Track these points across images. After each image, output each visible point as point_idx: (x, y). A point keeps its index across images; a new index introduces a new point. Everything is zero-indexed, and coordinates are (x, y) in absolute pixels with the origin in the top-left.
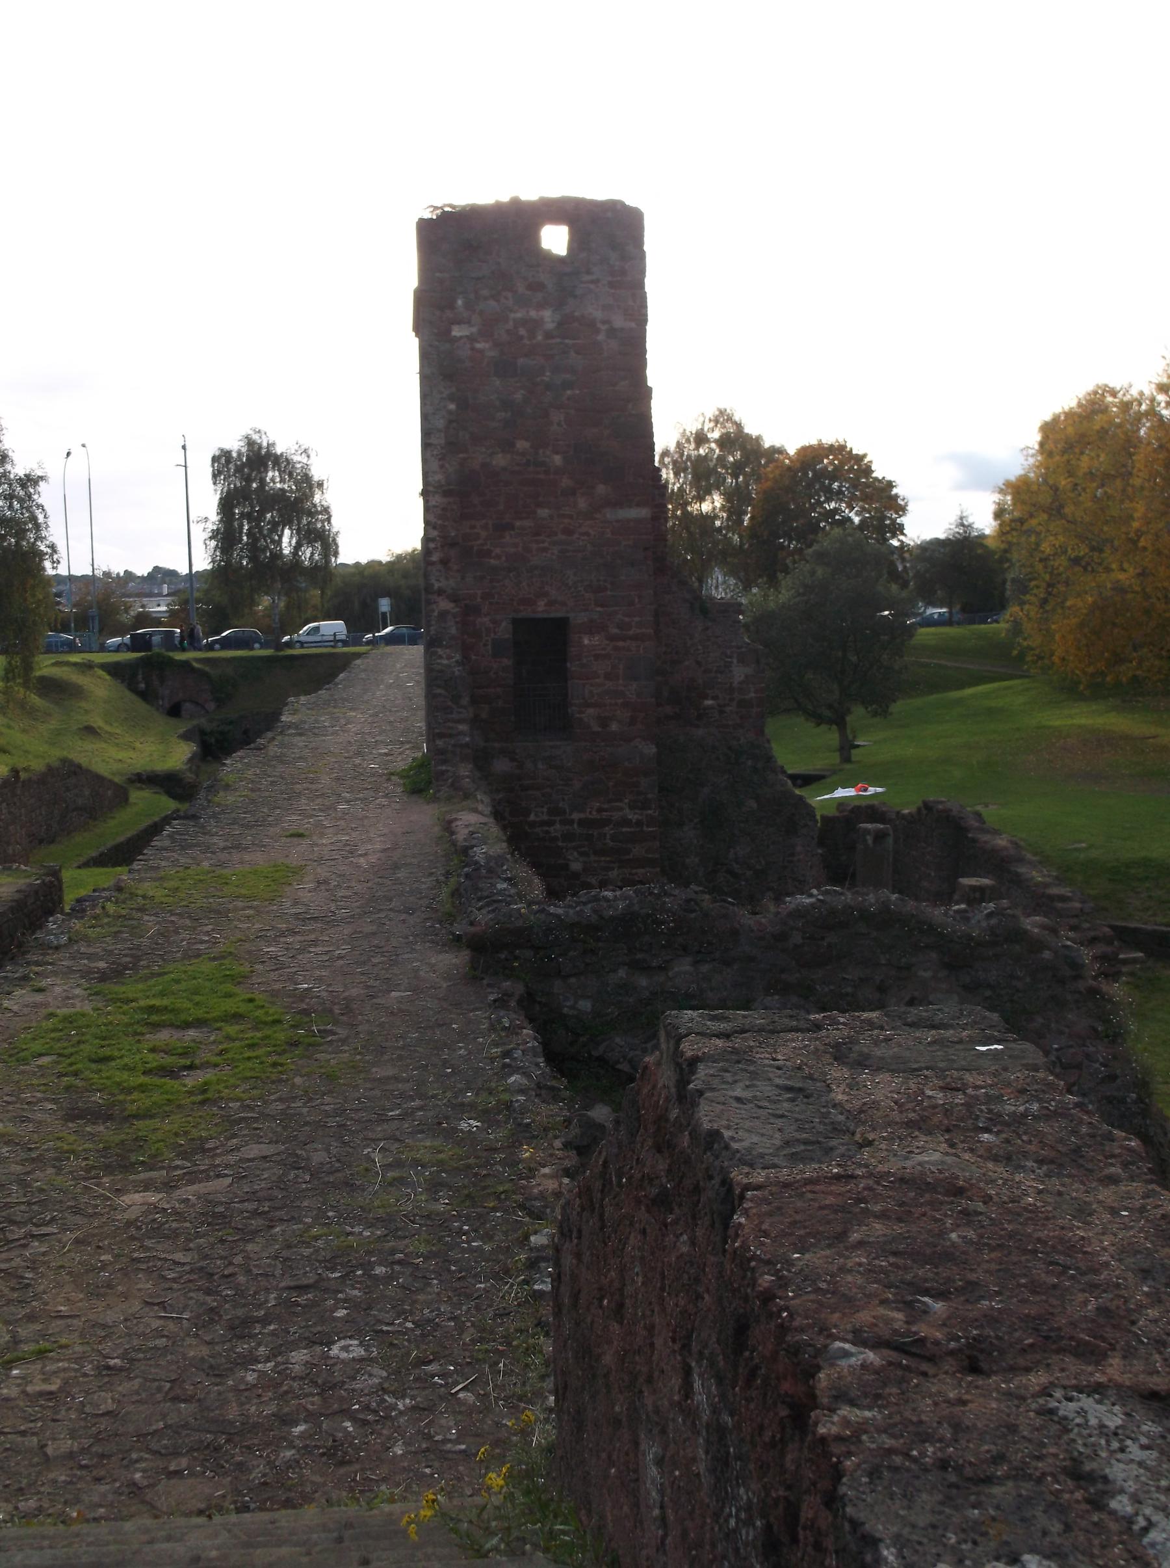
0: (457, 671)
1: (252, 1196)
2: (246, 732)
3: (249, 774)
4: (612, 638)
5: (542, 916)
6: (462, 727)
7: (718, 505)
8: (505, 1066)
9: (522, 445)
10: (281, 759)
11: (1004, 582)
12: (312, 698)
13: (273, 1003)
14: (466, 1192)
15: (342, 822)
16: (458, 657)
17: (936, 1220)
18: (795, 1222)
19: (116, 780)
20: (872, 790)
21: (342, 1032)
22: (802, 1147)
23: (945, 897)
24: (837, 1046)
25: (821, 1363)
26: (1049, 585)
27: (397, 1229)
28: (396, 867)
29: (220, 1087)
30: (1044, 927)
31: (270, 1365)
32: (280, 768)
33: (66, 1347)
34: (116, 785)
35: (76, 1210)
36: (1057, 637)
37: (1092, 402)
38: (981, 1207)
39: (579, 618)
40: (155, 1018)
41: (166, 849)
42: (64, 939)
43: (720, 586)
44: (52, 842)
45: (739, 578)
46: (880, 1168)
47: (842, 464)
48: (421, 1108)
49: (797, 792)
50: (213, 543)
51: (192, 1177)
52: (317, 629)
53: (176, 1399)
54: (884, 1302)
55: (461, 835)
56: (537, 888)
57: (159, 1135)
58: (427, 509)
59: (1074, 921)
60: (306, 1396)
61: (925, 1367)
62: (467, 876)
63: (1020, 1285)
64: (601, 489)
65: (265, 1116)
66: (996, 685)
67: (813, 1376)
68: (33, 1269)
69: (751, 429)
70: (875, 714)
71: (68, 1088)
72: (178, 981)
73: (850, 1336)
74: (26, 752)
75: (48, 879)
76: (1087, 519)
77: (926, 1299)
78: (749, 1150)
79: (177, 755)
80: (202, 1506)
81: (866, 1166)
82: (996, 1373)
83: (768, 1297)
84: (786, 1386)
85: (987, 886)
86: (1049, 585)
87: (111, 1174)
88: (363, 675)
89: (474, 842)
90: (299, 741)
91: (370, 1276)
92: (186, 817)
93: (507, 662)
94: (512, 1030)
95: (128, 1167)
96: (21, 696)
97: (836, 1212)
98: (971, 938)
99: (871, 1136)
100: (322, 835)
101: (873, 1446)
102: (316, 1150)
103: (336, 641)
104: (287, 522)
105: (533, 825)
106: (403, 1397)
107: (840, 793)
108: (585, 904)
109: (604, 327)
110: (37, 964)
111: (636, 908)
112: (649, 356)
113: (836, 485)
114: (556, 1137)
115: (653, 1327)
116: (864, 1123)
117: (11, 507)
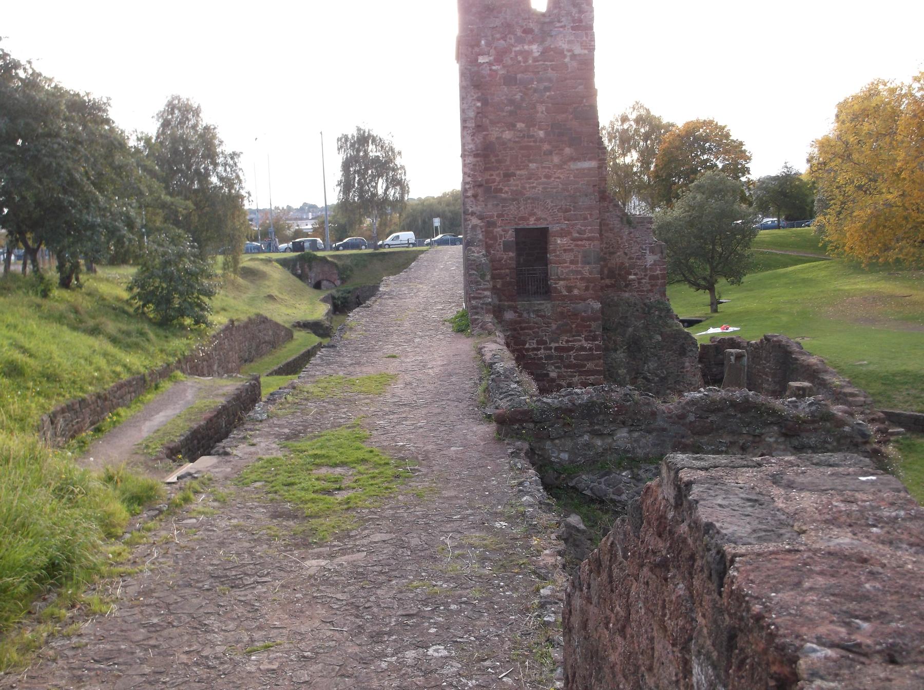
0: (483, 260)
1: (378, 563)
2: (358, 297)
3: (363, 321)
5: (539, 404)
6: (487, 293)
8: (520, 491)
9: (520, 125)
10: (380, 312)
11: (813, 202)
12: (397, 277)
13: (384, 453)
14: (501, 563)
15: (417, 349)
16: (484, 252)
17: (855, 577)
18: (769, 576)
19: (287, 325)
20: (731, 329)
21: (424, 470)
23: (779, 393)
24: (773, 476)
25: (800, 655)
27: (462, 584)
28: (450, 375)
29: (357, 501)
30: (845, 412)
32: (381, 318)
33: (280, 644)
34: (286, 329)
35: (281, 569)
37: (870, 90)
38: (881, 570)
40: (318, 461)
41: (318, 365)
42: (265, 416)
43: (636, 207)
44: (252, 361)
45: (647, 202)
46: (814, 546)
47: (711, 132)
49: (686, 330)
50: (339, 188)
51: (344, 552)
52: (398, 237)
53: (343, 676)
54: (832, 622)
55: (488, 357)
56: (534, 388)
57: (324, 527)
58: (464, 165)
59: (861, 409)
60: (416, 676)
61: (862, 659)
62: (493, 380)
63: (913, 615)
64: (568, 151)
65: (383, 518)
66: (807, 265)
67: (795, 662)
68: (259, 601)
69: (655, 112)
70: (733, 283)
71: (271, 500)
72: (329, 440)
73: (815, 641)
77: (857, 621)
78: (733, 534)
79: (320, 311)
81: (806, 545)
82: (906, 664)
83: (759, 618)
84: (774, 669)
85: (807, 387)
87: (299, 549)
89: (496, 360)
90: (390, 302)
91: (448, 610)
92: (329, 347)
94: (523, 470)
95: (307, 545)
97: (793, 570)
98: (798, 418)
99: (804, 528)
100: (406, 357)
102: (413, 537)
103: (409, 244)
104: (380, 175)
105: (527, 350)
106: (471, 679)
107: (712, 331)
108: (564, 396)
109: (569, 54)
110: (251, 430)
111: (595, 399)
112: (596, 70)
113: (707, 145)
114: (552, 533)
116: (798, 520)
117: (225, 170)
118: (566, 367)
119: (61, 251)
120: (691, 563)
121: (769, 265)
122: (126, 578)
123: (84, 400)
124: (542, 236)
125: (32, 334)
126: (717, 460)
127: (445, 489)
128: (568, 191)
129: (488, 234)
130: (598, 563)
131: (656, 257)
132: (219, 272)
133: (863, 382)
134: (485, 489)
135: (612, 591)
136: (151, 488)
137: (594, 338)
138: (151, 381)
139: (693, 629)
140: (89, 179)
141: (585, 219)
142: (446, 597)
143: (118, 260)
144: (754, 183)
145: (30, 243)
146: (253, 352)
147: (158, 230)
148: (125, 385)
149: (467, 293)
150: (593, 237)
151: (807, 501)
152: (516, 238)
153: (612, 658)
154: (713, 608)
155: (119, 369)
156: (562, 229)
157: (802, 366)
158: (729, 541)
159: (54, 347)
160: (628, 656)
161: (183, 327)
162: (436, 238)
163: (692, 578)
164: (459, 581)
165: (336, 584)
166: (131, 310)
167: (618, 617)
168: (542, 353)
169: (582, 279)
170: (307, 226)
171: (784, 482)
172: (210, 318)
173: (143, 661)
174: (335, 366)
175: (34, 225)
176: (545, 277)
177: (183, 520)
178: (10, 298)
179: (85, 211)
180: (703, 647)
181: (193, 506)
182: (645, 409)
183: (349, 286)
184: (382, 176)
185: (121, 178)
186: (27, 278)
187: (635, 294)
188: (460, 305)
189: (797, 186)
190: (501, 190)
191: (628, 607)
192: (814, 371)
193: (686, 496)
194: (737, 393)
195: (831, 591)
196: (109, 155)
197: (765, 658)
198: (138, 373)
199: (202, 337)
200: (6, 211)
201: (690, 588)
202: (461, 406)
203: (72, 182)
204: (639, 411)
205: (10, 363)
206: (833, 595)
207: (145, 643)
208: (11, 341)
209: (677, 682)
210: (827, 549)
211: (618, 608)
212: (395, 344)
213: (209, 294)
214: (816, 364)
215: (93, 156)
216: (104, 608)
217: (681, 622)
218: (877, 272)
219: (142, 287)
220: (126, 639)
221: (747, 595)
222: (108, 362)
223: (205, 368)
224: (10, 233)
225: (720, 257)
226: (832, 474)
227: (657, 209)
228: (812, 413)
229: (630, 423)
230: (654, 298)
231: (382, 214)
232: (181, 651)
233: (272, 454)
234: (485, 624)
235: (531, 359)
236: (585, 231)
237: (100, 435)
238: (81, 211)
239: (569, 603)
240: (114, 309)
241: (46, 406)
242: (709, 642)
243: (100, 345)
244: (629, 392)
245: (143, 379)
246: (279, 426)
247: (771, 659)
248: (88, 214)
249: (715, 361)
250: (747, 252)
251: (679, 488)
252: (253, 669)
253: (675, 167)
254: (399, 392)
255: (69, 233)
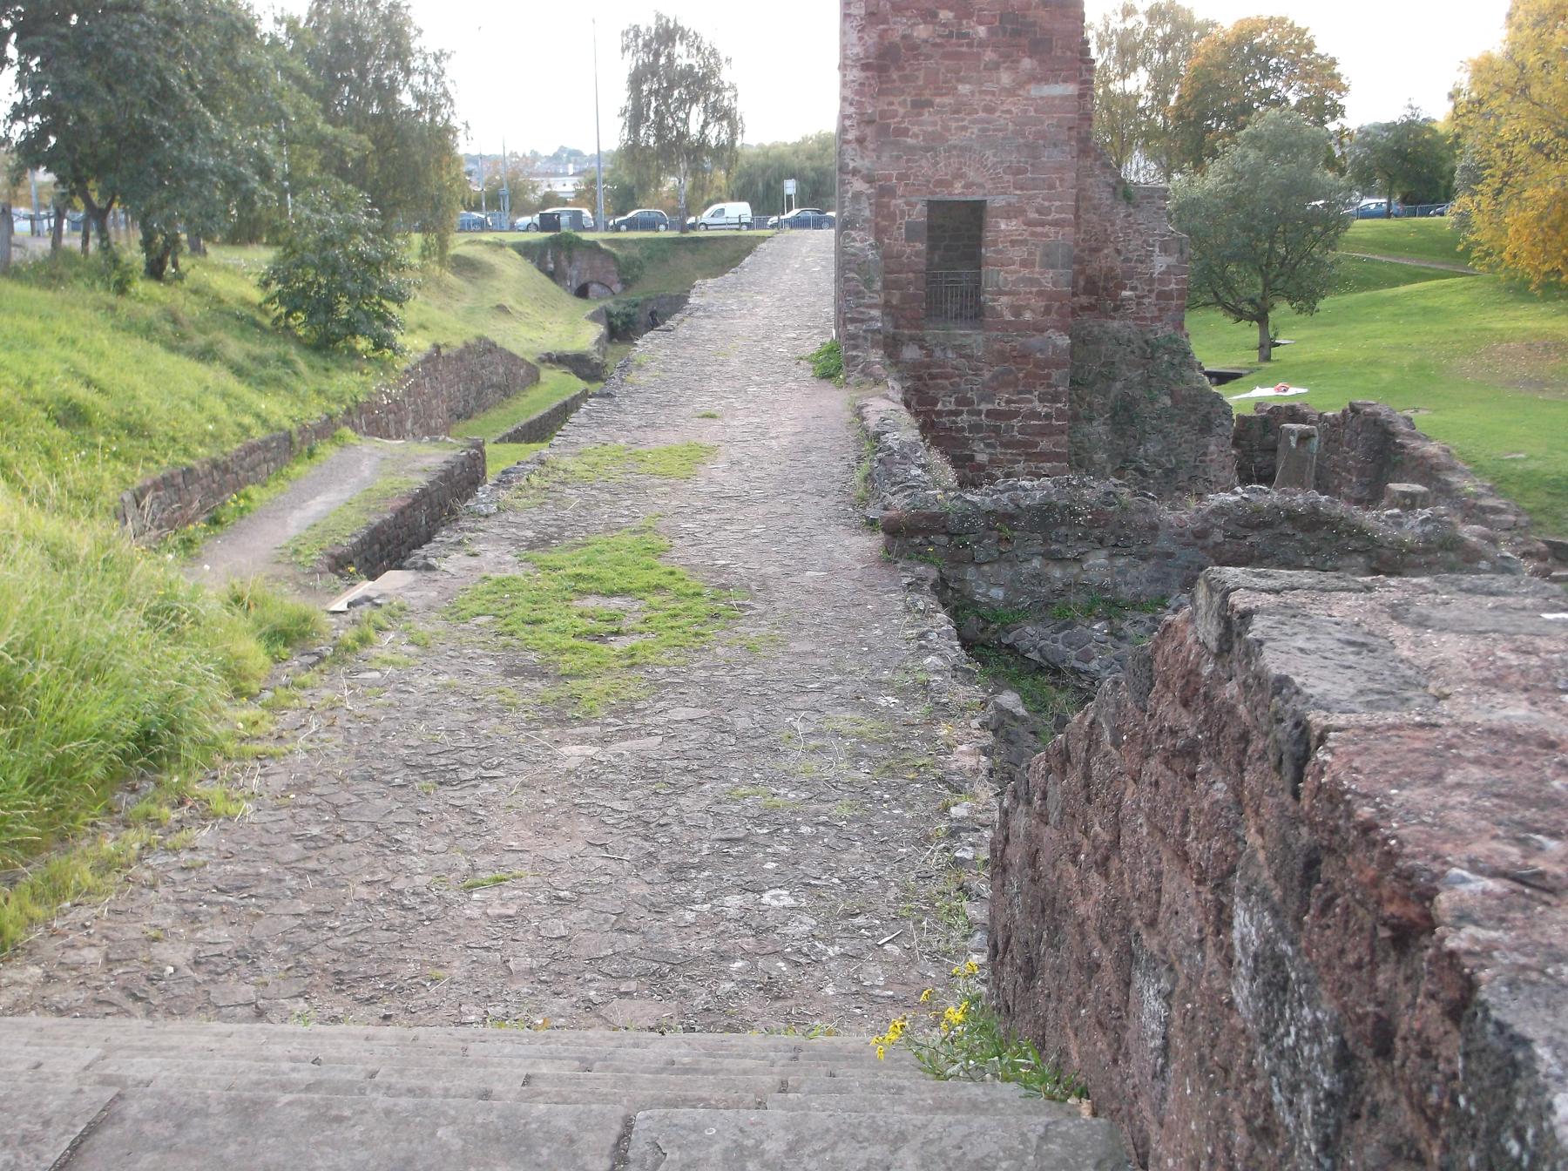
0: (871, 255)
3: (660, 355)
4: (1029, 224)
5: (958, 503)
6: (875, 313)
7: (1143, 83)
8: (921, 647)
9: (945, 15)
10: (689, 340)
11: (1453, 171)
14: (886, 763)
15: (752, 405)
16: (872, 240)
17: (1535, 769)
19: (529, 359)
20: (1292, 391)
21: (761, 607)
22: (1377, 697)
24: (1392, 606)
26: (1506, 174)
27: (821, 793)
28: (807, 451)
30: (1483, 537)
31: (707, 906)
32: (691, 350)
36: (1510, 232)
39: (997, 202)
40: (582, 585)
42: (493, 508)
43: (1139, 169)
44: (470, 417)
46: (1464, 719)
47: (1282, 38)
48: (839, 683)
49: (1214, 389)
51: (625, 734)
54: (1495, 837)
55: (872, 422)
56: (950, 476)
57: (592, 694)
58: (844, 85)
60: (741, 936)
61: (1546, 897)
64: (1027, 63)
66: (1434, 283)
67: (1431, 899)
70: (1300, 311)
71: (505, 647)
72: (601, 552)
73: (1466, 865)
74: (445, 329)
75: (473, 451)
76: (1555, 101)
77: (1539, 837)
78: (1324, 695)
79: (586, 336)
80: (652, 1025)
83: (1368, 828)
84: (1391, 909)
86: (1506, 174)
88: (769, 259)
92: (601, 396)
93: (920, 246)
95: (564, 722)
96: (437, 273)
97: (1427, 755)
98: (1402, 543)
99: (1447, 690)
100: (733, 417)
101: (1506, 962)
104: (694, 100)
105: (939, 414)
106: (833, 944)
107: (1259, 393)
108: (1002, 492)
110: (471, 530)
113: (1273, 62)
114: (973, 717)
115: (1160, 873)
116: (1437, 678)
117: (425, 82)
118: (1003, 445)
119: (147, 215)
120: (1242, 746)
121: (1370, 279)
122: (266, 762)
123: (190, 470)
124: (975, 213)
125: (102, 354)
126: (1295, 579)
127: (792, 639)
128: (1024, 136)
129: (880, 208)
130: (1065, 756)
131: (1172, 260)
132: (416, 261)
133: (1515, 490)
134: (861, 641)
135: (1089, 800)
136: (306, 620)
137: (1055, 399)
138: (302, 442)
139: (1238, 855)
140: (193, 88)
141: (1052, 187)
142: (794, 813)
143: (241, 236)
144: (1350, 135)
145: (95, 197)
146: (472, 402)
147: (313, 184)
148: (259, 448)
149: (839, 311)
150: (1064, 220)
151: (1451, 648)
152: (929, 216)
153: (1081, 910)
154: (1279, 818)
155: (247, 420)
156: (1009, 204)
157: (1413, 458)
158: (1317, 706)
159: (138, 380)
160: (1112, 905)
161: (354, 354)
162: (788, 216)
163: (1243, 771)
164: (817, 790)
165: (611, 785)
166: (267, 322)
167: (1098, 843)
168: (964, 420)
169: (1040, 294)
170: (565, 186)
171: (1412, 617)
172: (400, 340)
173: (297, 894)
174: (611, 429)
175: (102, 168)
176: (977, 288)
177: (359, 672)
178: (64, 293)
179: (187, 146)
180: (1256, 882)
181: (374, 652)
182: (1140, 519)
183: (637, 295)
184: (697, 101)
185: (248, 88)
186: (90, 260)
187: (1130, 323)
188: (824, 333)
189: (1427, 141)
190: (905, 132)
191: (1117, 826)
192: (1432, 467)
193: (1239, 635)
194: (1300, 498)
195: (1495, 790)
196: (227, 48)
197: (1375, 892)
198: (281, 429)
199: (386, 372)
200: (53, 140)
201: (1236, 789)
202: (824, 502)
203: (166, 93)
204: (1129, 523)
205: (66, 403)
206: (1498, 796)
207: (300, 865)
208: (66, 366)
209: (1201, 941)
210: (1487, 725)
211: (1097, 828)
212: (713, 394)
213: (399, 298)
214: (1436, 456)
215: (201, 48)
216: (232, 808)
217: (1216, 845)
218: (1556, 299)
219: (285, 281)
220: (268, 858)
221: (1348, 791)
222: (229, 407)
223: (392, 424)
224: (62, 180)
225: (1282, 265)
226: (1496, 608)
227: (1176, 176)
228: (1425, 534)
229: (1113, 542)
230: (1163, 331)
231: (696, 170)
232: (359, 880)
233: (505, 571)
234: (856, 858)
235: (945, 429)
236: (1049, 208)
237: (218, 529)
238: (181, 146)
239: (1005, 825)
240: (238, 318)
241: (129, 479)
242: (1266, 874)
243: (216, 378)
244: (1112, 488)
245: (288, 438)
246: (517, 526)
247: (1385, 893)
248: (193, 151)
249: (1260, 445)
250: (1331, 255)
251: (1227, 623)
252: (476, 913)
253: (1213, 102)
254: (718, 475)
255: (161, 184)
